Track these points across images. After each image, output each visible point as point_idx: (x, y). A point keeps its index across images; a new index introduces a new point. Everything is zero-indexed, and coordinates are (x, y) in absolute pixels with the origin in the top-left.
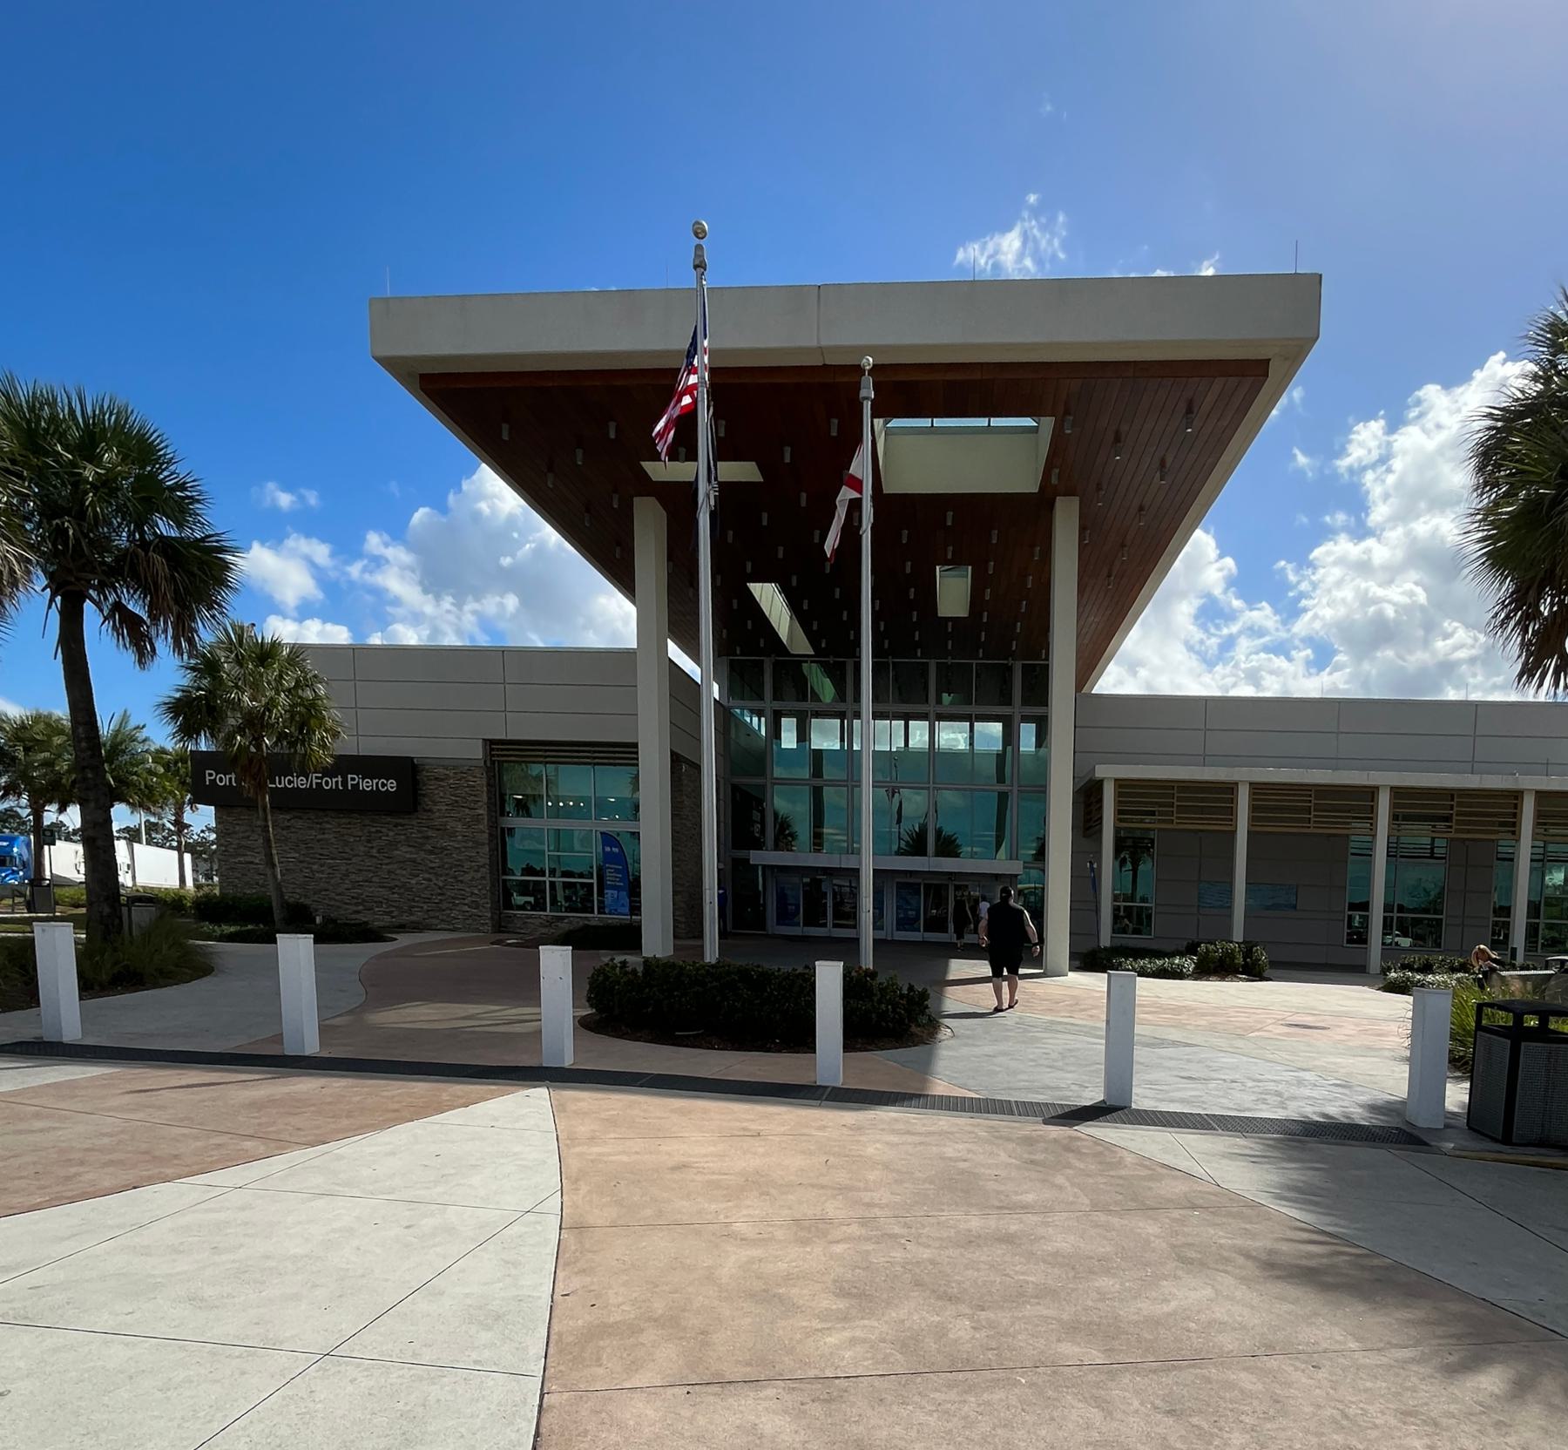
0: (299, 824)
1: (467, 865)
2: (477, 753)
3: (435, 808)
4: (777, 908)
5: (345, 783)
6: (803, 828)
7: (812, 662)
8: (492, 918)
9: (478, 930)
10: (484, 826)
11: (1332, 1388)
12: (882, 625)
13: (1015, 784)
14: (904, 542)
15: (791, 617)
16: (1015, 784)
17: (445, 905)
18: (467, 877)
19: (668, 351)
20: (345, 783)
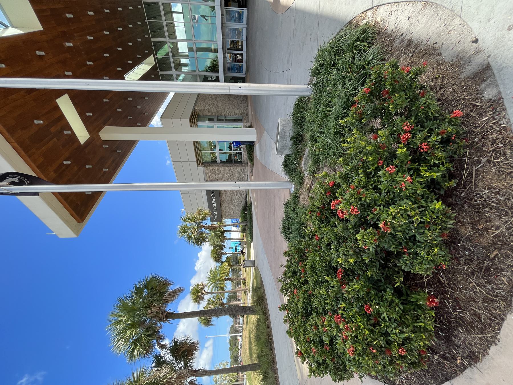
0: (224, 205)
1: (231, 172)
2: (201, 169)
3: (217, 178)
4: (232, 181)
5: (213, 197)
6: (211, 55)
7: (157, 55)
8: (244, 166)
9: (247, 170)
10: (220, 168)
11: (347, 290)
12: (138, 124)
13: (187, 3)
14: (108, 146)
15: (143, 63)
16: (187, 3)
17: (241, 177)
18: (234, 172)
19: (60, 217)
20: (213, 197)
